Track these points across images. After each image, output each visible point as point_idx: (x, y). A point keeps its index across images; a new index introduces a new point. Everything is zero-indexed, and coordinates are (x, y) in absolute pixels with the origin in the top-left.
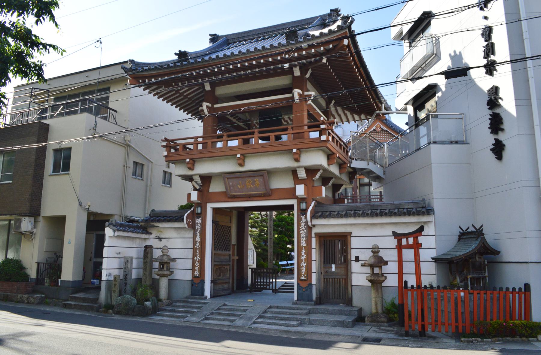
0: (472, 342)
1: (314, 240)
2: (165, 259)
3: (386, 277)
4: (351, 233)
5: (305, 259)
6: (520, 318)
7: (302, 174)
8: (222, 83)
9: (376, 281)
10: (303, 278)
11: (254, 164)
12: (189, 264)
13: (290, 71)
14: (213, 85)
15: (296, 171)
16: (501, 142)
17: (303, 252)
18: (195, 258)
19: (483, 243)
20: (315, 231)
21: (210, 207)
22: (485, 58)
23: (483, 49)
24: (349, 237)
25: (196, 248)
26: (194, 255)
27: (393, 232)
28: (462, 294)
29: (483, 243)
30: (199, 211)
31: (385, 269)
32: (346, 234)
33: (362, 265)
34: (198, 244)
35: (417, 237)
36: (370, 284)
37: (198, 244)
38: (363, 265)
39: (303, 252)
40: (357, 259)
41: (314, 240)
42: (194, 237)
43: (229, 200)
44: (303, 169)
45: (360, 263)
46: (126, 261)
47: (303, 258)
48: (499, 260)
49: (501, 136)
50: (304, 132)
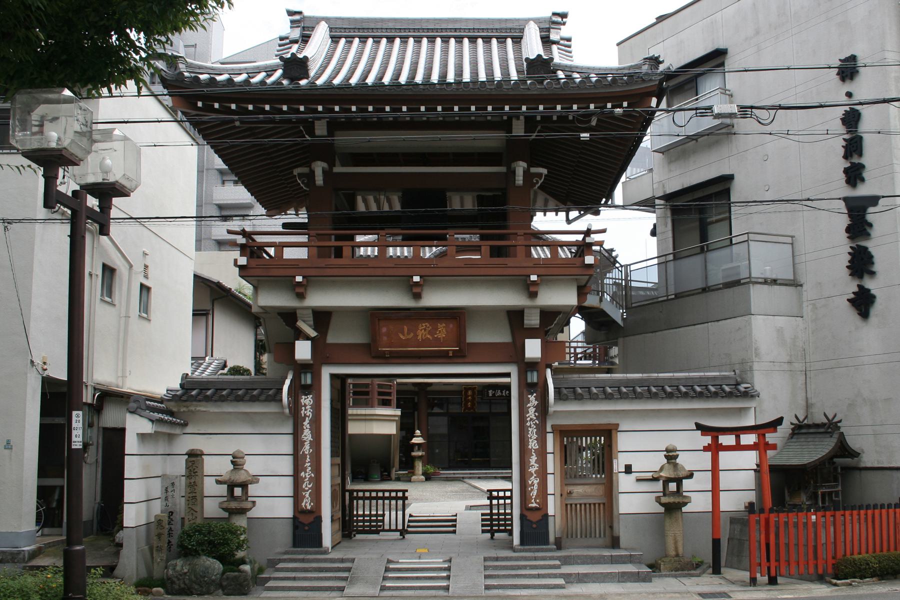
0: (851, 585)
1: (550, 438)
2: (241, 477)
3: (254, 502)
4: (618, 425)
6: (889, 550)
7: (533, 320)
8: (351, 125)
9: (673, 507)
10: (534, 505)
12: (286, 486)
13: (506, 126)
14: (334, 126)
16: (869, 290)
17: (533, 459)
18: (303, 474)
19: (841, 442)
21: (326, 372)
22: (846, 157)
23: (844, 144)
24: (614, 432)
25: (304, 455)
26: (297, 466)
27: (697, 424)
28: (814, 517)
29: (841, 442)
30: (309, 381)
32: (609, 428)
33: (638, 480)
35: (764, 435)
36: (662, 510)
39: (533, 459)
40: (628, 469)
41: (550, 438)
43: (374, 361)
46: (168, 483)
48: (862, 465)
49: (870, 284)
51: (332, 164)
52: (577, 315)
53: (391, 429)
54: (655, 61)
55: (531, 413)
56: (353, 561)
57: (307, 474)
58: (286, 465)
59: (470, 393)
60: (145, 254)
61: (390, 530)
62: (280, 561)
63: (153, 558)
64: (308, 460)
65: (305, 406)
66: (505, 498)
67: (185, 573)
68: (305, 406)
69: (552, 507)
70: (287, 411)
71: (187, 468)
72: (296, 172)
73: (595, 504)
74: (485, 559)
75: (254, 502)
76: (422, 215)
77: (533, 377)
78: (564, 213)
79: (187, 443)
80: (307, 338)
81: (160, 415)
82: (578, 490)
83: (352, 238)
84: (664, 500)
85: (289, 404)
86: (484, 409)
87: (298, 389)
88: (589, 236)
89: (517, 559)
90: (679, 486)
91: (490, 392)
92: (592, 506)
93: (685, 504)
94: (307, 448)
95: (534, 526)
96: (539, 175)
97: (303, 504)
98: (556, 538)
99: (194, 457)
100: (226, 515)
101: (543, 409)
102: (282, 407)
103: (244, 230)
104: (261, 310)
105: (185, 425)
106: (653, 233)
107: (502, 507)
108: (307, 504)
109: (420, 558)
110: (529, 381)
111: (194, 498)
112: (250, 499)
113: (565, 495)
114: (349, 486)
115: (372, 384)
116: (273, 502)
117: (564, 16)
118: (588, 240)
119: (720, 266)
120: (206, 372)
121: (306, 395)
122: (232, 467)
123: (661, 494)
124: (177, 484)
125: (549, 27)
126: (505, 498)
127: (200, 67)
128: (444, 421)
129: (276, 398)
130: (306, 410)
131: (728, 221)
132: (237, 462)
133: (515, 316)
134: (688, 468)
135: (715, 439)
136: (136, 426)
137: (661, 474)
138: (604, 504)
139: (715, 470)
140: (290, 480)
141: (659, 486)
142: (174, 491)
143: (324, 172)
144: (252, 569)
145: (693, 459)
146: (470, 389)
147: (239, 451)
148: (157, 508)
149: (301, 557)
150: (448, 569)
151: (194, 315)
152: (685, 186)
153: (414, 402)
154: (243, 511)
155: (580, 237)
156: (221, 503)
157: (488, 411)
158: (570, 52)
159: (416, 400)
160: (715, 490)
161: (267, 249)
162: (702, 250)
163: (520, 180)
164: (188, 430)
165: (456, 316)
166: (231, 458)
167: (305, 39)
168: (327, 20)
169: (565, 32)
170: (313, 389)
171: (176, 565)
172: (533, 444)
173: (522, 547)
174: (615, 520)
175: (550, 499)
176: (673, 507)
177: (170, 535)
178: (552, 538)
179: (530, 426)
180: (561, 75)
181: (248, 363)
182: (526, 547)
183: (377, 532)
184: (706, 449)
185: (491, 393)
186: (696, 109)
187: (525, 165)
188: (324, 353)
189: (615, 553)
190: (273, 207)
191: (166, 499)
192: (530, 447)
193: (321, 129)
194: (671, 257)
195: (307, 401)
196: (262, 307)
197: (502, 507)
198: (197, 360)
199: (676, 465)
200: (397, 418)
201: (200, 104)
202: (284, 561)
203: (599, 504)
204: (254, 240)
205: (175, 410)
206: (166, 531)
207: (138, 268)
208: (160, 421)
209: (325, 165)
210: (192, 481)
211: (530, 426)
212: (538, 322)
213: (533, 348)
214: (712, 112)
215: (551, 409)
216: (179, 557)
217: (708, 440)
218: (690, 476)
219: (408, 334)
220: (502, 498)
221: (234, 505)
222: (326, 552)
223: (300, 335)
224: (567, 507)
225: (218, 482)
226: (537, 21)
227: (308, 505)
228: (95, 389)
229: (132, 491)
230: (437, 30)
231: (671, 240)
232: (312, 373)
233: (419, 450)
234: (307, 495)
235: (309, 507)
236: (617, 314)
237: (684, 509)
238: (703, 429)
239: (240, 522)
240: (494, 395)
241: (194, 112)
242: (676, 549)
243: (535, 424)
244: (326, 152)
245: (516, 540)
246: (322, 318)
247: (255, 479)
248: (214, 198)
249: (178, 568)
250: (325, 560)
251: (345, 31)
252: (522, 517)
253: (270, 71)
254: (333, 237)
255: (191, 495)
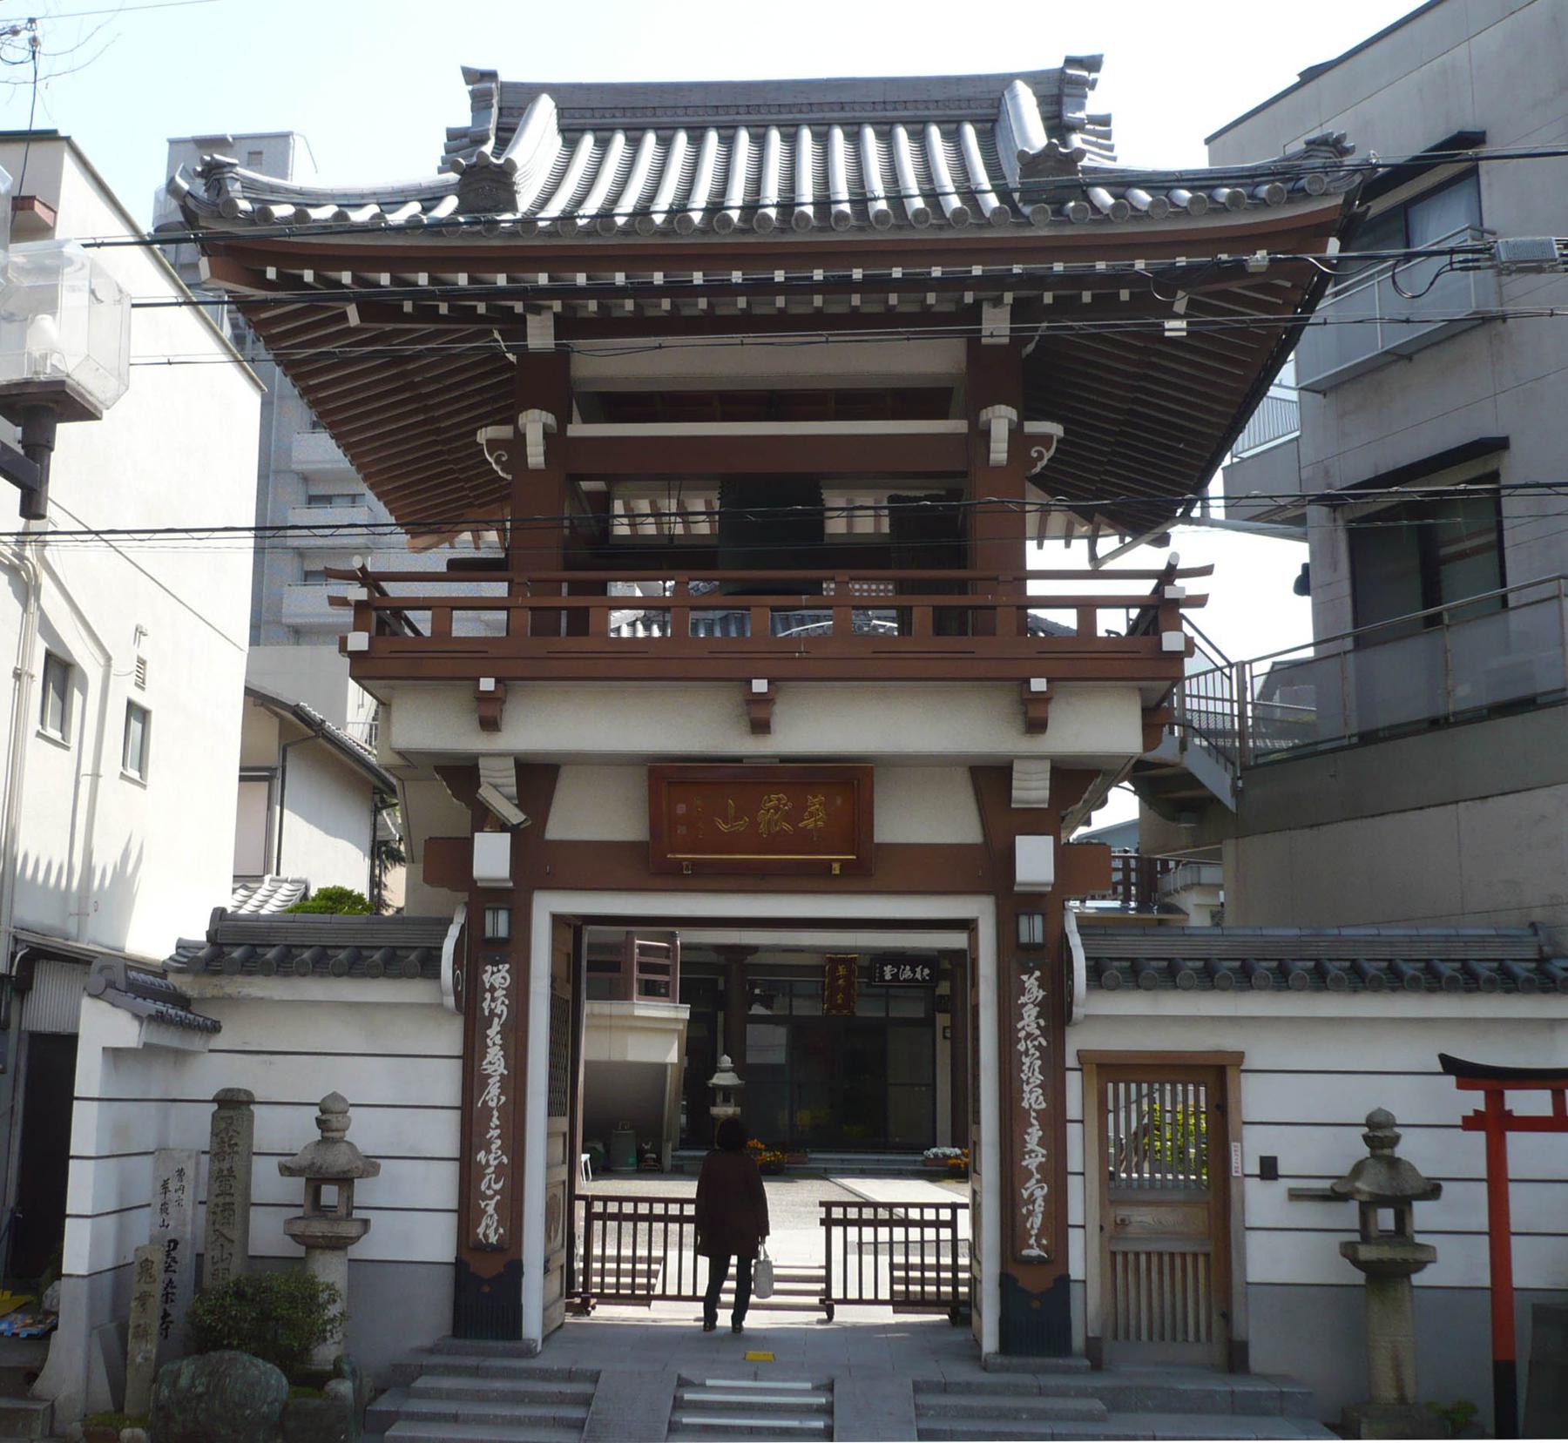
2: (337, 1159)
4: (1240, 1056)
5: (1040, 1167)
7: (1032, 788)
8: (607, 326)
9: (1386, 1267)
10: (1035, 1252)
11: (817, 727)
12: (441, 1185)
15: (476, 768)
17: (1034, 1134)
18: (481, 1156)
20: (1077, 1041)
21: (546, 906)
24: (1230, 1073)
27: (1444, 1058)
30: (503, 931)
31: (1423, 1214)
34: (494, 1089)
36: (1359, 1277)
37: (494, 1089)
38: (1295, 1196)
39: (1034, 1134)
40: (1269, 1169)
41: (1074, 1081)
42: (471, 1056)
44: (511, 762)
45: (1282, 1186)
47: (1031, 1163)
50: (994, 608)
51: (564, 419)
52: (1126, 784)
53: (671, 1054)
54: (1335, 146)
55: (1030, 1019)
56: (594, 1378)
57: (491, 1157)
58: (442, 1134)
59: (841, 970)
60: (140, 632)
61: (679, 1298)
62: (422, 1370)
63: (125, 1353)
64: (495, 1122)
65: (493, 989)
66: (938, 1224)
67: (200, 1396)
68: (493, 989)
69: (1081, 1260)
70: (450, 1001)
71: (214, 1134)
72: (483, 436)
73: (1183, 1255)
74: (918, 1388)
75: (366, 1222)
76: (769, 537)
77: (1032, 930)
78: (1085, 542)
79: (213, 1072)
80: (503, 827)
81: (160, 1006)
82: (1142, 1217)
83: (603, 591)
84: (1367, 1253)
85: (456, 983)
86: (867, 1010)
87: (477, 950)
88: (1171, 583)
89: (995, 1391)
90: (1402, 1218)
91: (888, 969)
92: (1155, 1259)
93: (1420, 1266)
94: (493, 1094)
95: (1036, 1304)
96: (1045, 440)
97: (480, 1230)
98: (1088, 1339)
99: (233, 1107)
100: (300, 1251)
101: (1058, 1012)
102: (442, 993)
103: (363, 569)
104: (398, 761)
105: (215, 1028)
106: (1303, 585)
107: (930, 1249)
108: (489, 1229)
109: (756, 1378)
110: (1024, 939)
111: (228, 1207)
112: (357, 1214)
113: (1109, 1228)
114: (585, 1186)
115: (629, 944)
116: (412, 1221)
117: (1093, 64)
118: (1169, 593)
119: (1478, 660)
120: (270, 900)
121: (496, 964)
122: (316, 1134)
123: (1356, 1237)
124: (190, 1172)
125: (1062, 90)
126: (938, 1224)
127: (273, 189)
128: (780, 1034)
129: (428, 966)
130: (493, 999)
131: (1494, 554)
132: (330, 1116)
133: (990, 779)
134: (1426, 1170)
135: (1495, 1099)
136: (103, 1027)
137: (1359, 1185)
138: (1207, 1255)
139: (1497, 1180)
140: (450, 1172)
141: (1348, 1215)
142: (182, 1189)
143: (547, 435)
144: (358, 1391)
145: (1440, 1148)
146: (843, 961)
147: (335, 1097)
148: (143, 1228)
149: (471, 1361)
150: (827, 1410)
151: (242, 779)
152: (1382, 471)
153: (719, 988)
154: (338, 1244)
155: (1145, 588)
156: (289, 1222)
157: (882, 1014)
158: (1111, 148)
159: (721, 986)
160: (1499, 1232)
161: (410, 614)
162: (1433, 621)
163: (999, 451)
164: (219, 1041)
165: (849, 781)
166: (316, 1112)
167: (507, 133)
168: (554, 90)
169: (1095, 104)
170: (514, 950)
171: (178, 1375)
172: (1033, 1098)
173: (1006, 1361)
174: (1237, 1299)
175: (1075, 1239)
176: (1386, 1267)
177: (167, 1297)
178: (1078, 1341)
179: (1026, 1053)
180: (1104, 197)
181: (359, 884)
182: (1015, 1361)
183: (646, 1300)
184: (1470, 1123)
185: (888, 971)
186: (1452, 252)
187: (1012, 413)
188: (539, 861)
189: (1242, 1386)
190: (423, 522)
191: (164, 1208)
192: (1025, 1104)
193: (540, 335)
194: (1349, 644)
195: (497, 977)
196: (400, 753)
197: (930, 1249)
198: (244, 881)
199: (1394, 1163)
200: (681, 1027)
201: (271, 273)
202: (432, 1370)
203: (1195, 1256)
204: (383, 593)
205: (192, 993)
206: (157, 1289)
207: (124, 664)
208: (159, 1019)
209: (549, 418)
210: (226, 1165)
211: (1026, 1053)
212: (1046, 793)
213: (1034, 860)
214: (1493, 257)
215: (1078, 1012)
216: (187, 1355)
217: (1475, 1100)
218: (1432, 1190)
219: (737, 819)
220: (930, 1224)
221: (318, 1228)
222: (529, 1352)
223: (485, 818)
224: (1116, 1259)
225: (286, 1170)
226: (1032, 79)
227: (491, 1232)
228: (16, 940)
229: (84, 1187)
230: (798, 108)
231: (1348, 601)
232: (510, 910)
233: (726, 1100)
234: (490, 1210)
235: (493, 1239)
236: (1218, 781)
237: (1417, 1279)
238: (1464, 1072)
239: (330, 1271)
240: (895, 977)
241: (260, 294)
242: (1400, 1385)
243: (1039, 1048)
244: (548, 382)
245: (990, 1342)
246: (538, 777)
247: (370, 1165)
248: (295, 454)
249: (184, 1382)
250: (530, 1374)
251: (594, 113)
252: (1006, 1282)
253: (431, 198)
254: (565, 588)
255: (221, 1200)
